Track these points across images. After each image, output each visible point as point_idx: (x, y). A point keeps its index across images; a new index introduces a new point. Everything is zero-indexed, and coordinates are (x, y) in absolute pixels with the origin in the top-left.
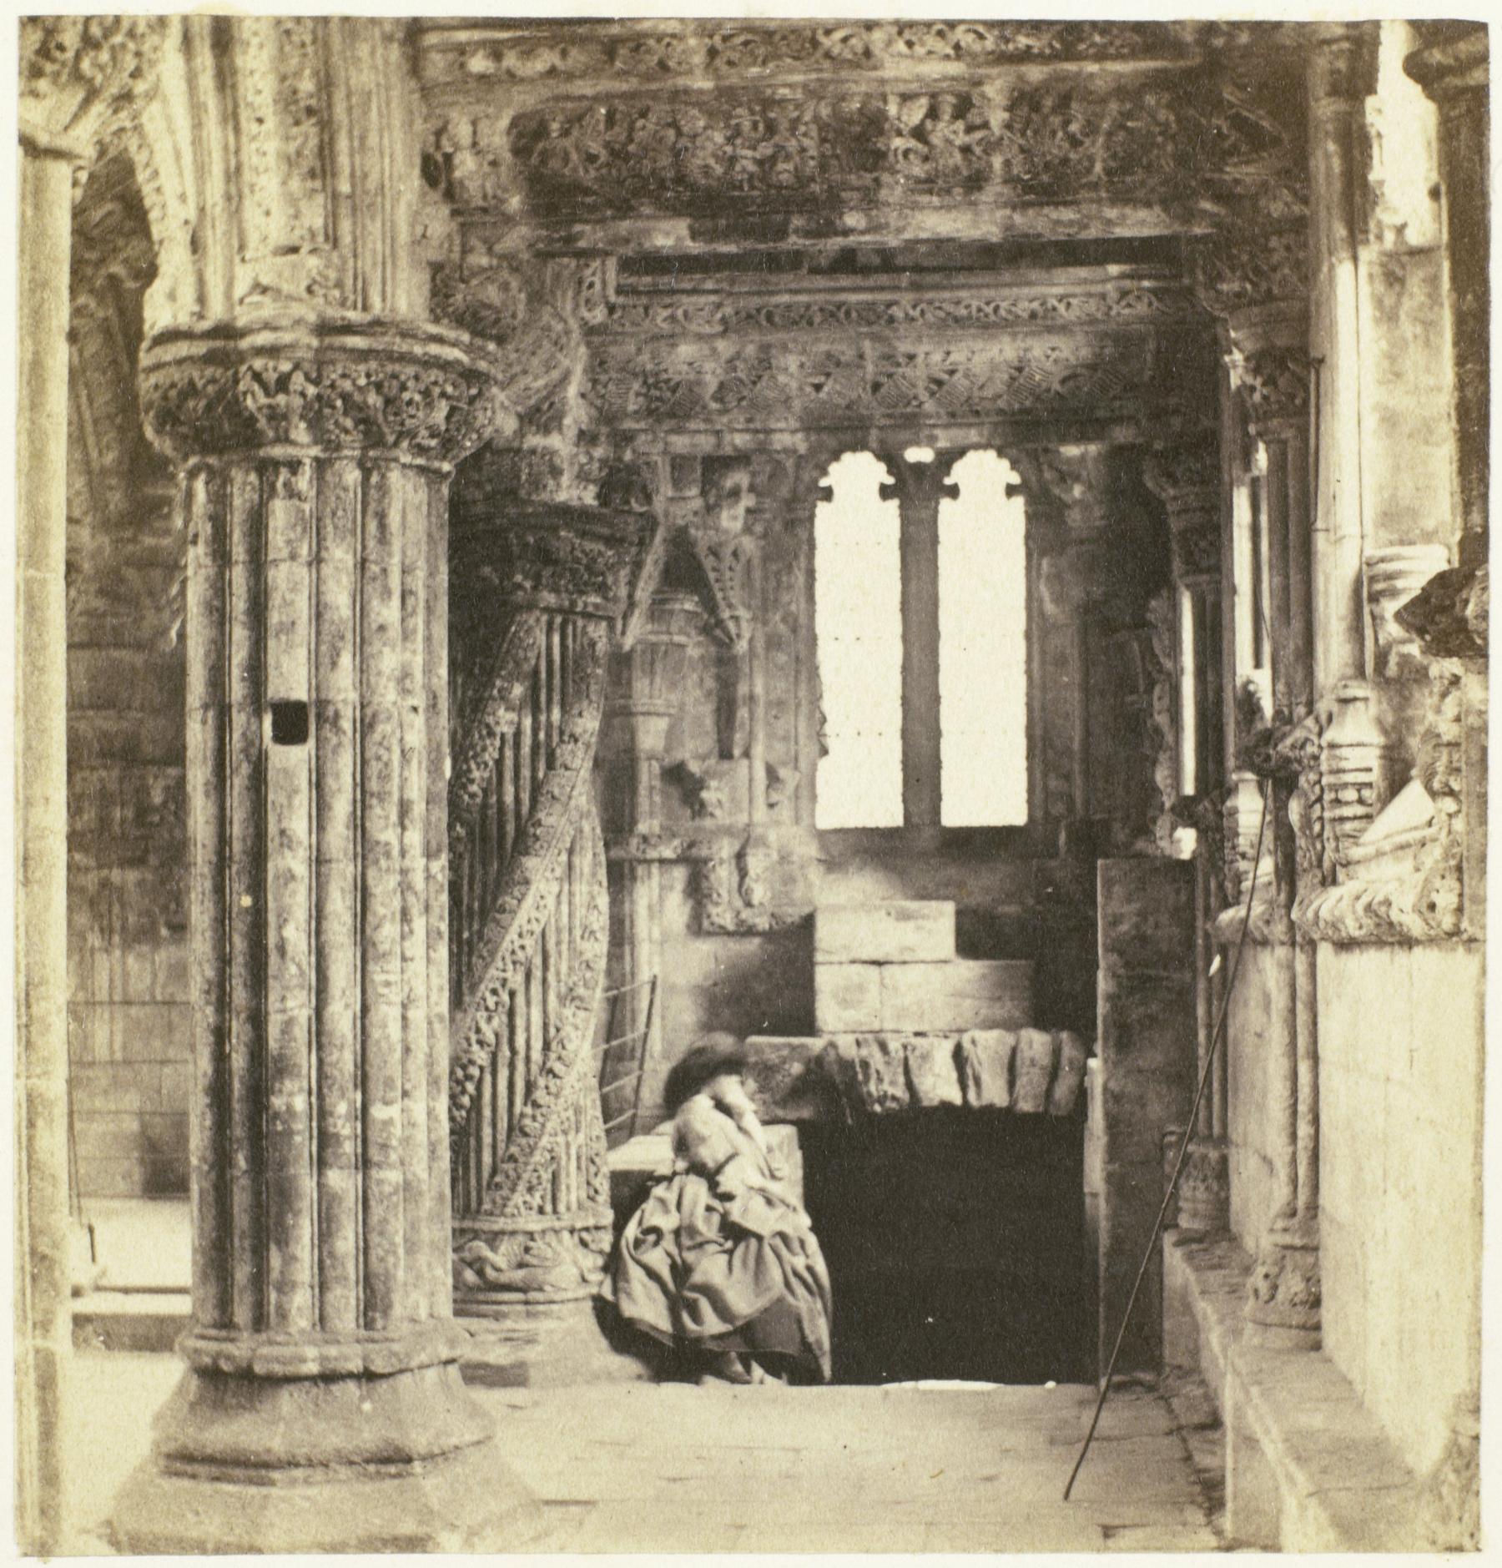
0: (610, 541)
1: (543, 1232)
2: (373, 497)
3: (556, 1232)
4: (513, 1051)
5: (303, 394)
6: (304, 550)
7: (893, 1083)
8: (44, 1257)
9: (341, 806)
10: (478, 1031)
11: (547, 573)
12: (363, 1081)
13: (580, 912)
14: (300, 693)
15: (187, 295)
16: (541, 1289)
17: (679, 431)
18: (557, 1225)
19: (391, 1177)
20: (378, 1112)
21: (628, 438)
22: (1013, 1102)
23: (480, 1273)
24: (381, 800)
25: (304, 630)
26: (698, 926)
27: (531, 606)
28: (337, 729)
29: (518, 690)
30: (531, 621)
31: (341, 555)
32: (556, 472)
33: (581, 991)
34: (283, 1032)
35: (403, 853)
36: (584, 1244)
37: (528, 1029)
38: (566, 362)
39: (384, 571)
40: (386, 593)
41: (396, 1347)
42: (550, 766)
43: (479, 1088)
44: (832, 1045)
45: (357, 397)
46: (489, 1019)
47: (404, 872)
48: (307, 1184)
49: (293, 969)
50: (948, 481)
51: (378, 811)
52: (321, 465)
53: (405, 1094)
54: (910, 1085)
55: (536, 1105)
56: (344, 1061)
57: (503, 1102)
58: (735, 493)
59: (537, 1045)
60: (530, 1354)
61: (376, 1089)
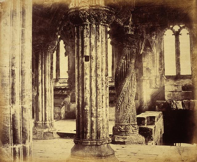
0: (136, 39)
1: (128, 125)
2: (97, 29)
3: (130, 125)
4: (124, 102)
5: (87, 15)
6: (88, 36)
7: (174, 106)
8: (24, 132)
9: (93, 69)
10: (120, 100)
11: (127, 43)
12: (97, 106)
13: (133, 84)
14: (88, 54)
15: (74, 4)
16: (127, 132)
17: (144, 25)
18: (130, 124)
19: (100, 119)
20: (98, 110)
21: (138, 26)
22: (189, 109)
23: (120, 130)
24: (99, 69)
25: (88, 47)
26: (150, 87)
27: (125, 47)
28: (93, 59)
29: (124, 57)
30: (126, 49)
31: (93, 36)
32: (129, 30)
33: (133, 95)
34: (86, 99)
35: (102, 76)
36: (133, 126)
37: (126, 100)
38: (156, 41)
39: (99, 38)
40: (99, 41)
41: (101, 141)
42: (128, 67)
43: (120, 107)
44: (167, 102)
45: (94, 15)
46: (121, 98)
47: (102, 78)
48: (89, 119)
49: (87, 91)
50: (180, 33)
51: (98, 70)
52: (90, 25)
53: (102, 108)
54: (176, 107)
55: (127, 109)
56: (94, 103)
57: (123, 109)
58: (154, 35)
59: (127, 101)
60: (126, 140)
61: (98, 107)
